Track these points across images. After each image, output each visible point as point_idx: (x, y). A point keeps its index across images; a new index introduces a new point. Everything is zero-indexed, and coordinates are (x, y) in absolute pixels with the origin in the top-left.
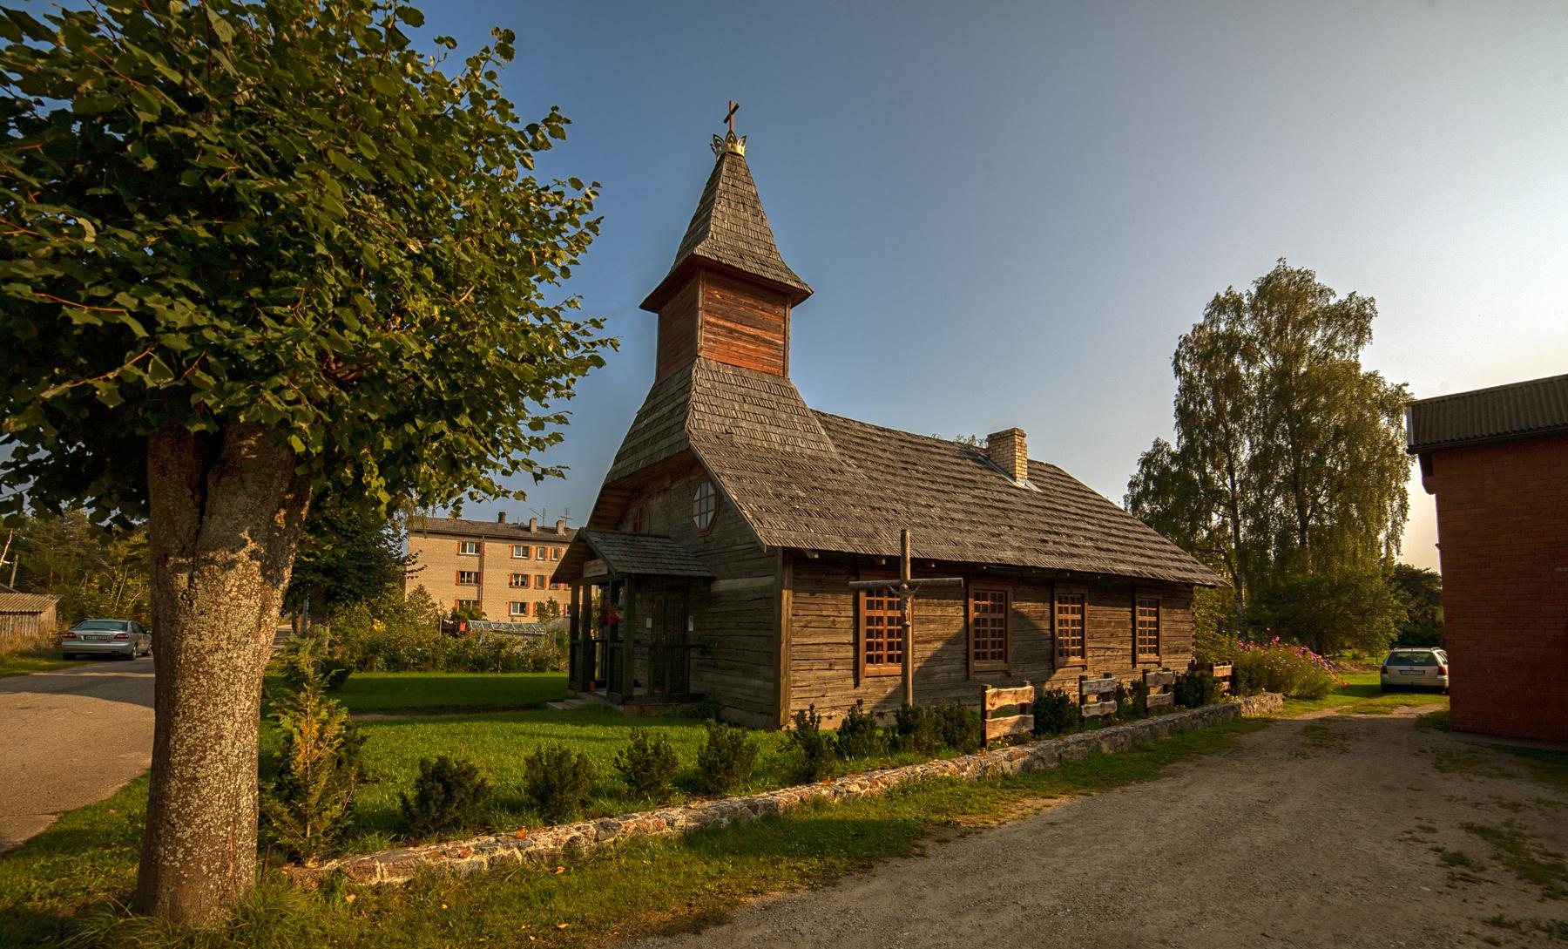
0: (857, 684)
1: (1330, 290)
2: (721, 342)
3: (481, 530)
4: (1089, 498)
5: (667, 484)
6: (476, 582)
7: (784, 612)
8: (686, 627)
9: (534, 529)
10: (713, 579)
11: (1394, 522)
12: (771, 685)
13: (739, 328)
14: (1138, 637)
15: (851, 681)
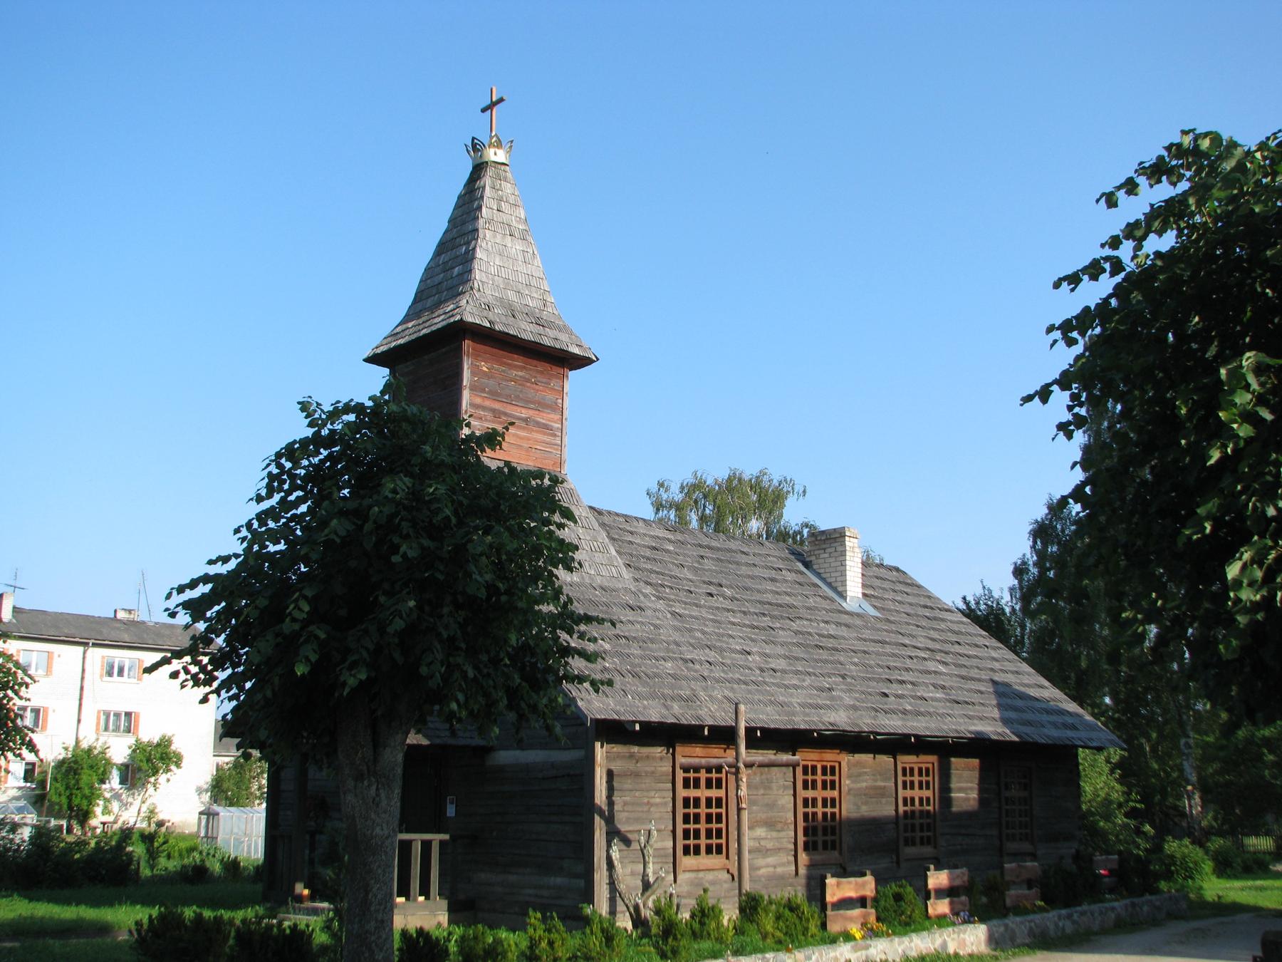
4: (943, 620)
10: (487, 750)
12: (582, 883)
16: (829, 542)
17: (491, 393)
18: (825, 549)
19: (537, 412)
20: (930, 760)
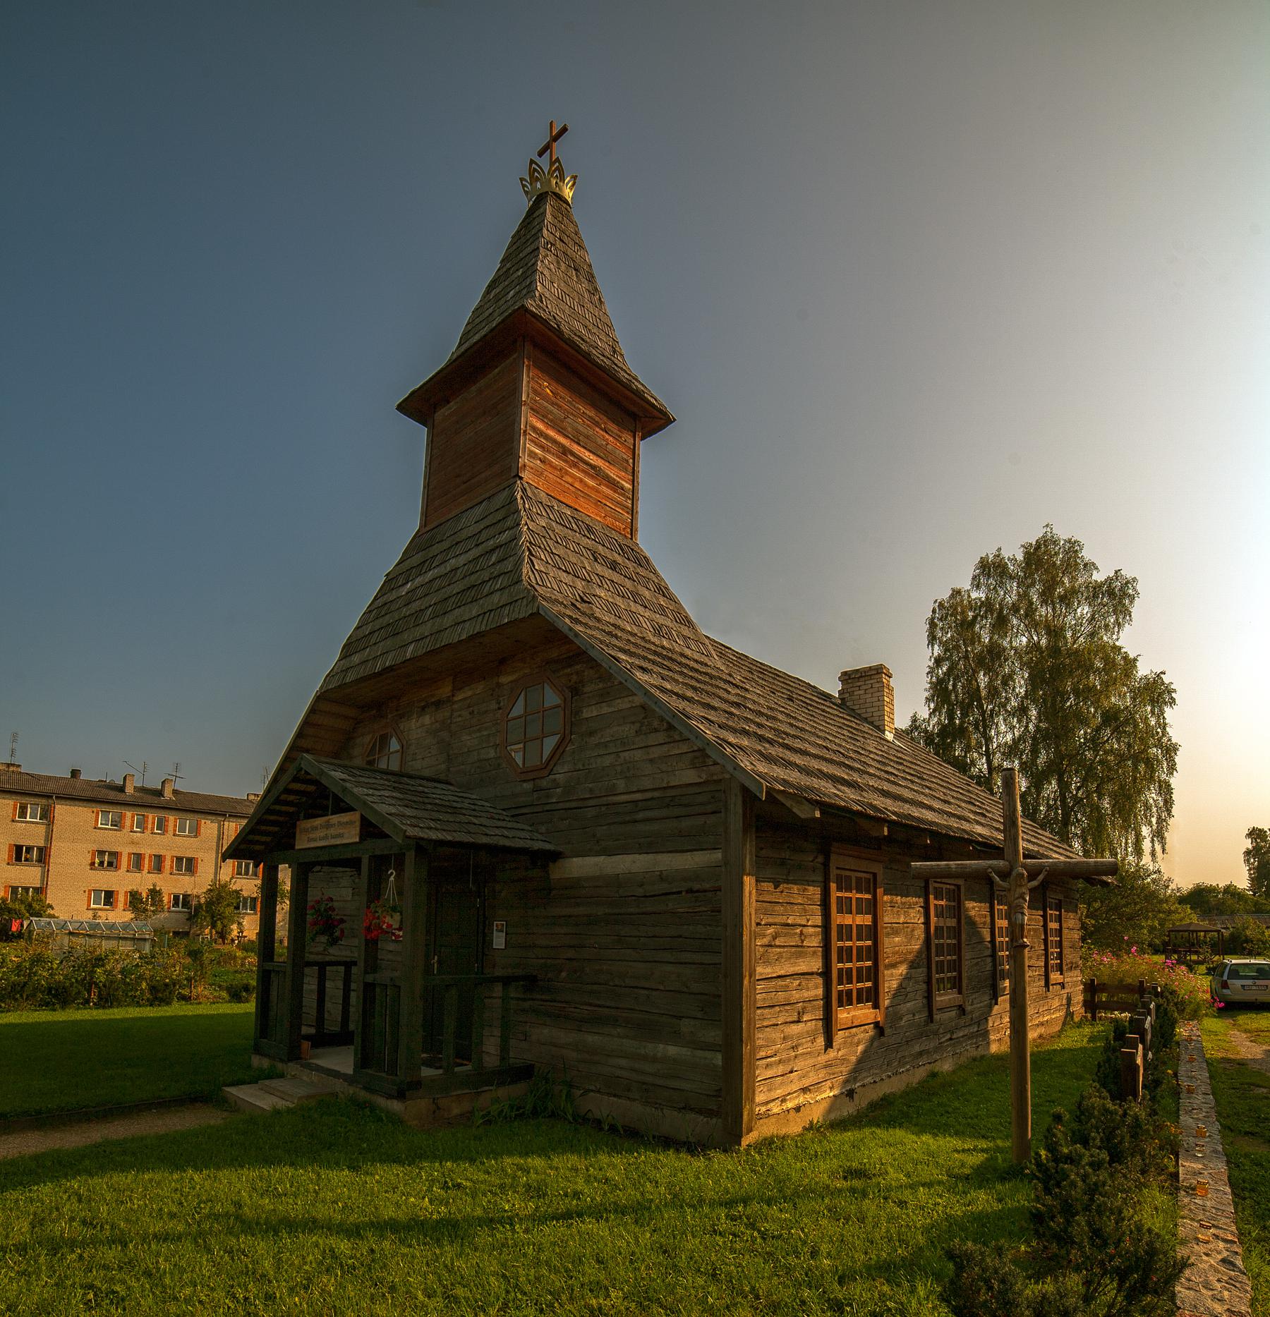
0: (829, 1044)
1: (1093, 564)
2: (550, 464)
3: (50, 787)
5: (445, 690)
6: (39, 860)
7: (746, 919)
8: (486, 942)
9: (129, 790)
10: (555, 856)
11: (1159, 818)
13: (576, 448)
14: (836, 944)
15: (821, 1041)
20: (342, 969)
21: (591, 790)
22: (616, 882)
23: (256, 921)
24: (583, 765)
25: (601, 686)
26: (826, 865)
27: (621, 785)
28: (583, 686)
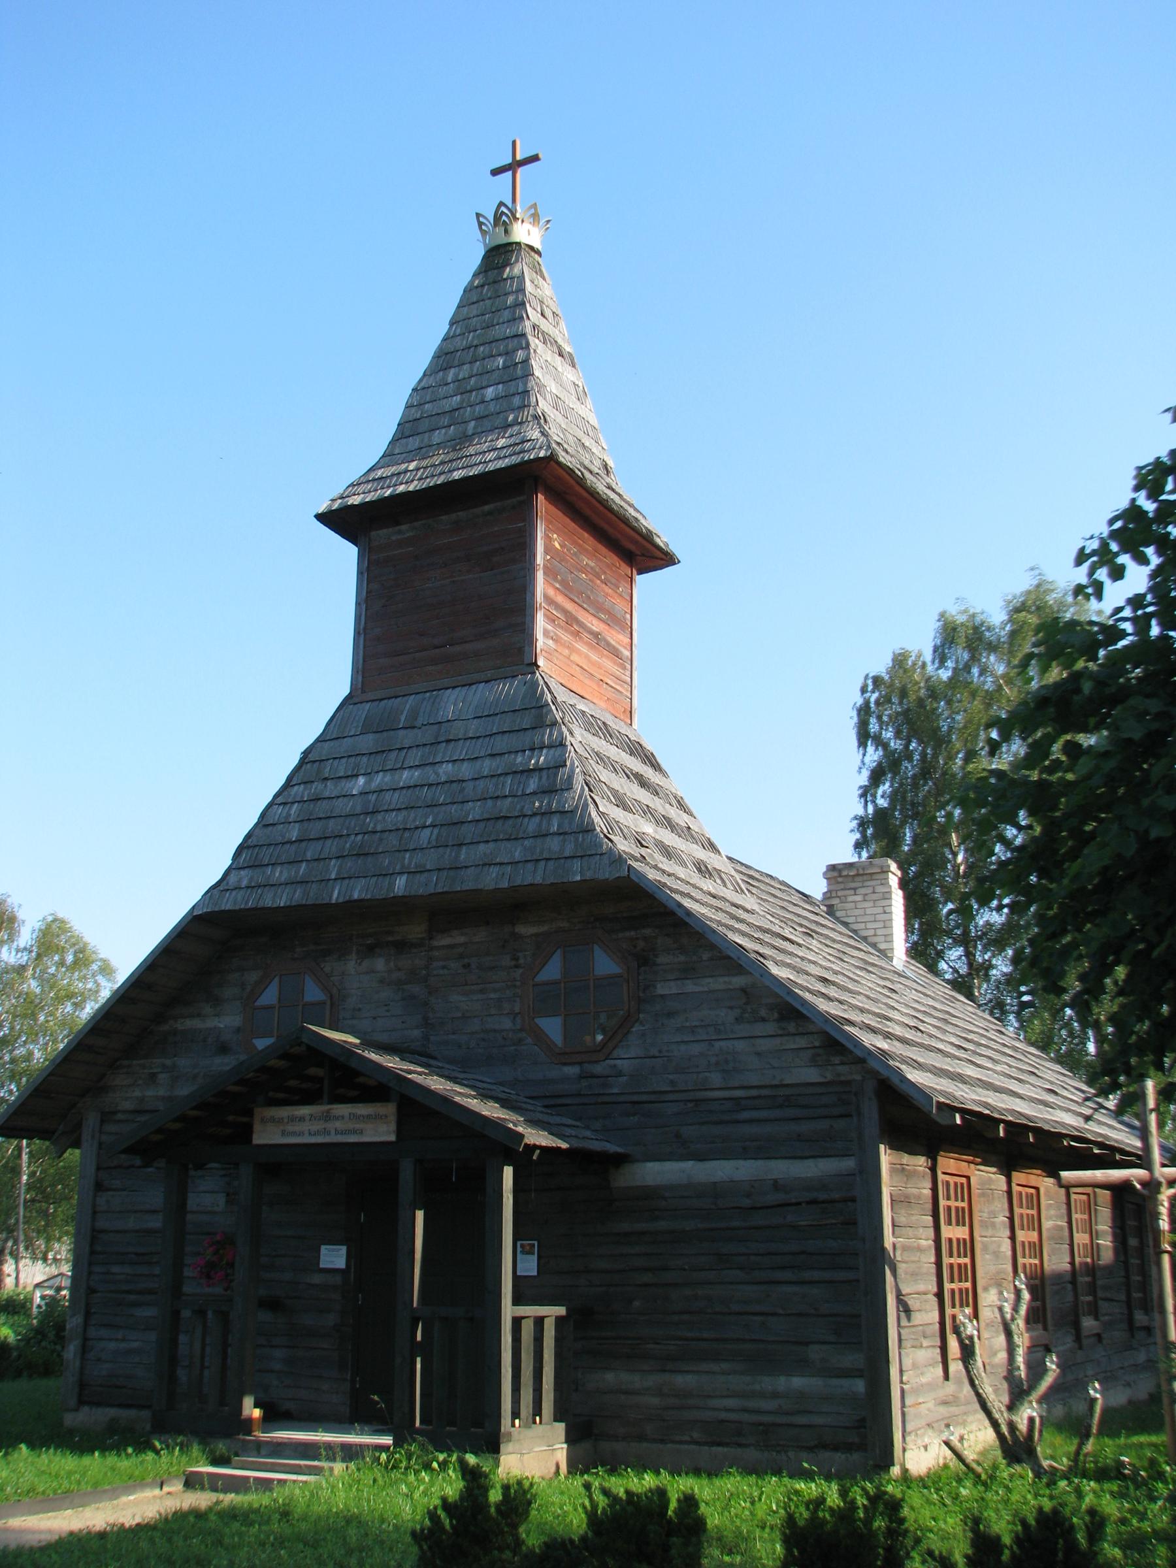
10: (620, 1160)
16: (860, 878)
17: (564, 583)
18: (855, 889)
19: (607, 627)
21: (672, 1082)
22: (714, 1190)
23: (329, 1250)
24: (660, 1051)
25: (682, 958)
26: (933, 1169)
27: (716, 1079)
28: (656, 956)
